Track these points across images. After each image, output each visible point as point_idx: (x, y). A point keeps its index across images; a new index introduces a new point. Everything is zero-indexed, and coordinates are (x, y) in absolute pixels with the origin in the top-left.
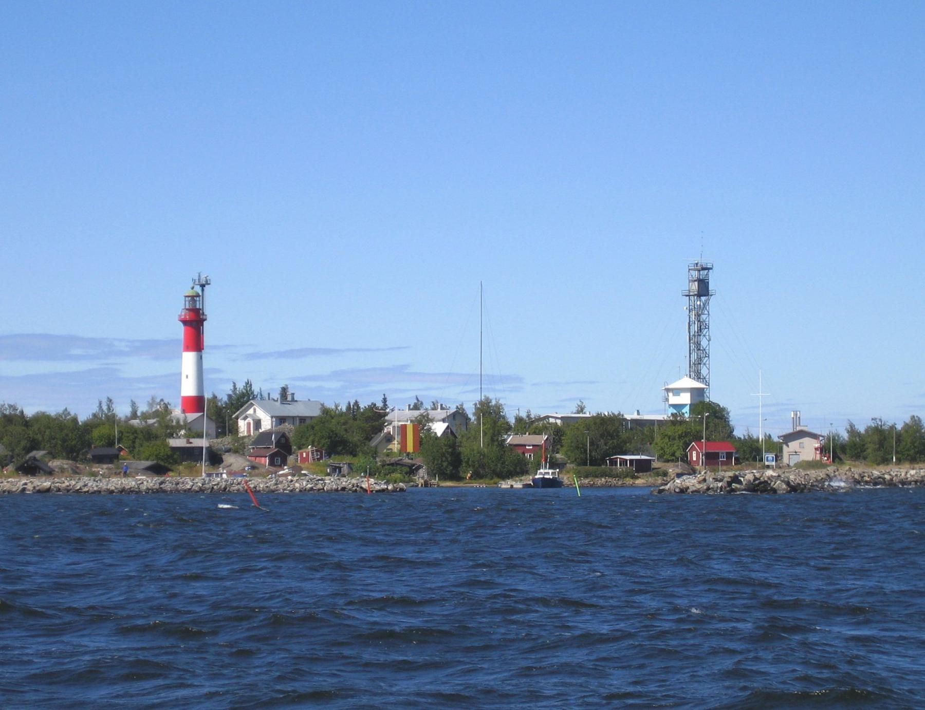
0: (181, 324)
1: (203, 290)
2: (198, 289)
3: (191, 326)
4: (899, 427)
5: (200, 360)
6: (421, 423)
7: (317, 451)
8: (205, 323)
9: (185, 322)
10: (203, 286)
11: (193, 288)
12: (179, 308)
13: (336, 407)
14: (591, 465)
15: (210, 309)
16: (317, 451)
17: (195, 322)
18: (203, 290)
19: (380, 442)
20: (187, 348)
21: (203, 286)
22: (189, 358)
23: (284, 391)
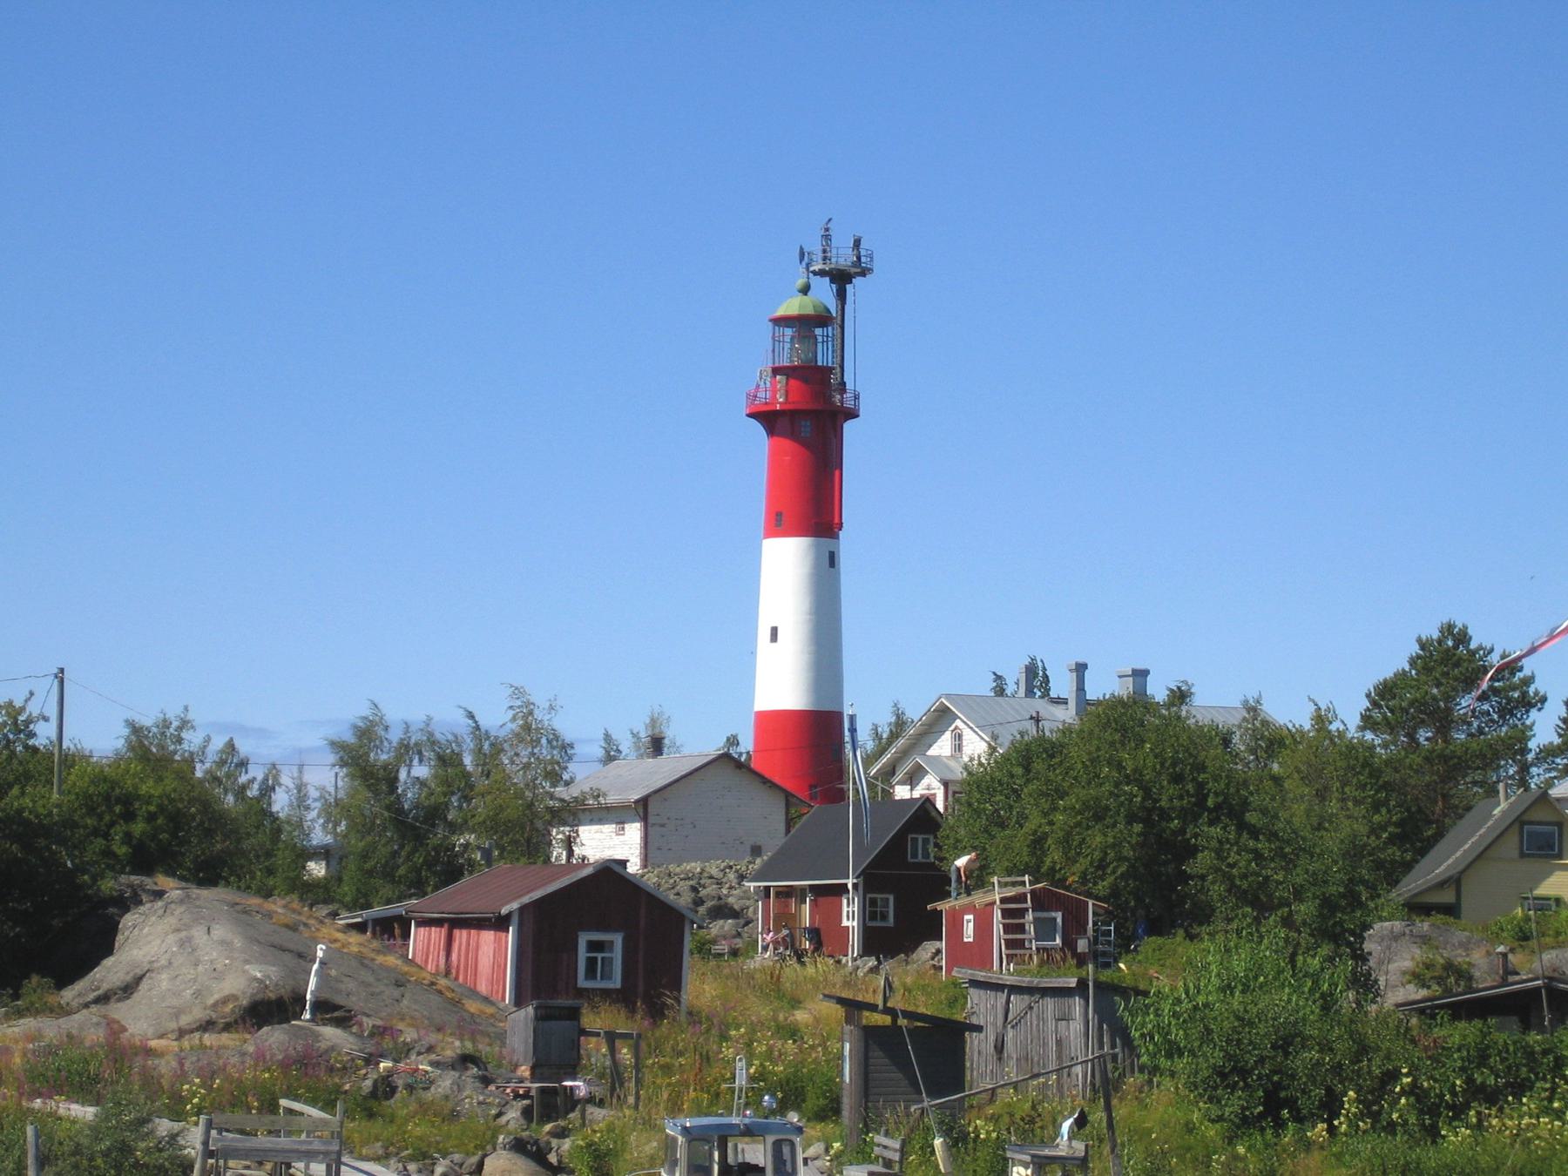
0: (757, 428)
1: (841, 296)
2: (824, 293)
3: (793, 435)
4: (1349, 715)
5: (827, 568)
6: (267, 790)
7: (1042, 901)
8: (849, 427)
9: (768, 418)
10: (841, 279)
11: (805, 290)
12: (751, 364)
13: (1321, 720)
14: (589, 959)
15: (866, 372)
16: (1042, 901)
17: (809, 422)
18: (841, 296)
19: (1482, 855)
20: (778, 525)
21: (841, 279)
22: (785, 560)
23: (1031, 671)
